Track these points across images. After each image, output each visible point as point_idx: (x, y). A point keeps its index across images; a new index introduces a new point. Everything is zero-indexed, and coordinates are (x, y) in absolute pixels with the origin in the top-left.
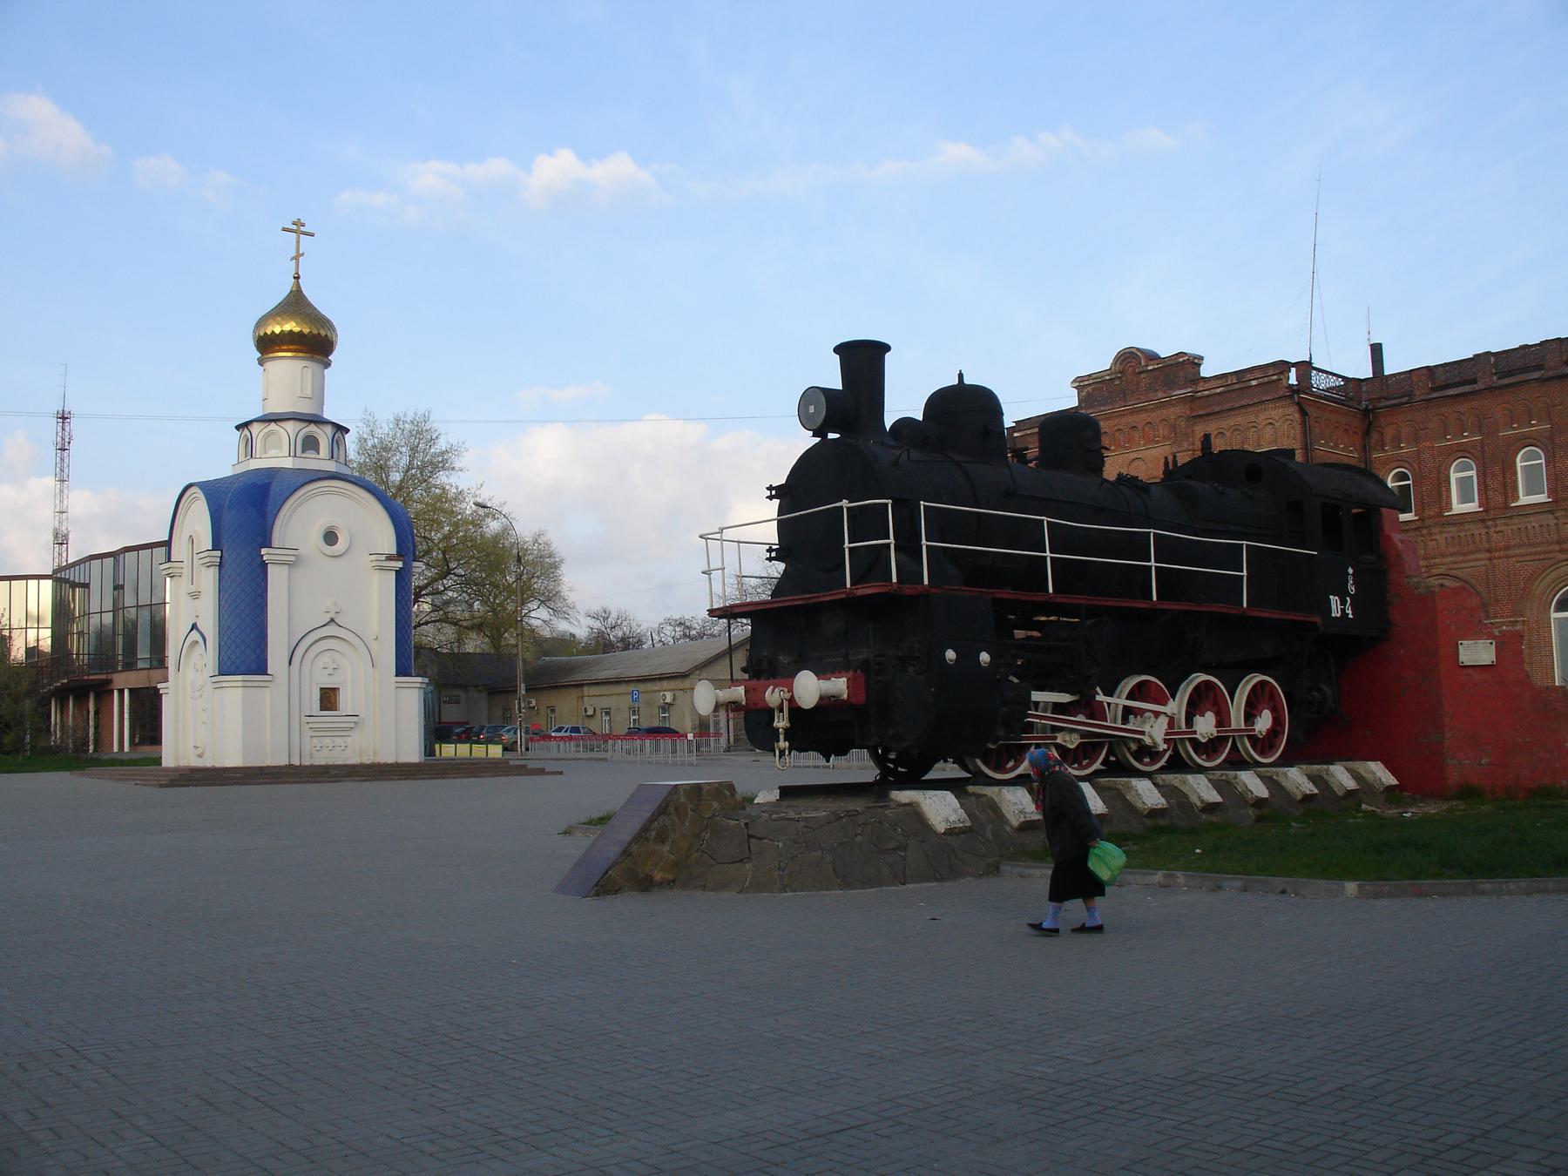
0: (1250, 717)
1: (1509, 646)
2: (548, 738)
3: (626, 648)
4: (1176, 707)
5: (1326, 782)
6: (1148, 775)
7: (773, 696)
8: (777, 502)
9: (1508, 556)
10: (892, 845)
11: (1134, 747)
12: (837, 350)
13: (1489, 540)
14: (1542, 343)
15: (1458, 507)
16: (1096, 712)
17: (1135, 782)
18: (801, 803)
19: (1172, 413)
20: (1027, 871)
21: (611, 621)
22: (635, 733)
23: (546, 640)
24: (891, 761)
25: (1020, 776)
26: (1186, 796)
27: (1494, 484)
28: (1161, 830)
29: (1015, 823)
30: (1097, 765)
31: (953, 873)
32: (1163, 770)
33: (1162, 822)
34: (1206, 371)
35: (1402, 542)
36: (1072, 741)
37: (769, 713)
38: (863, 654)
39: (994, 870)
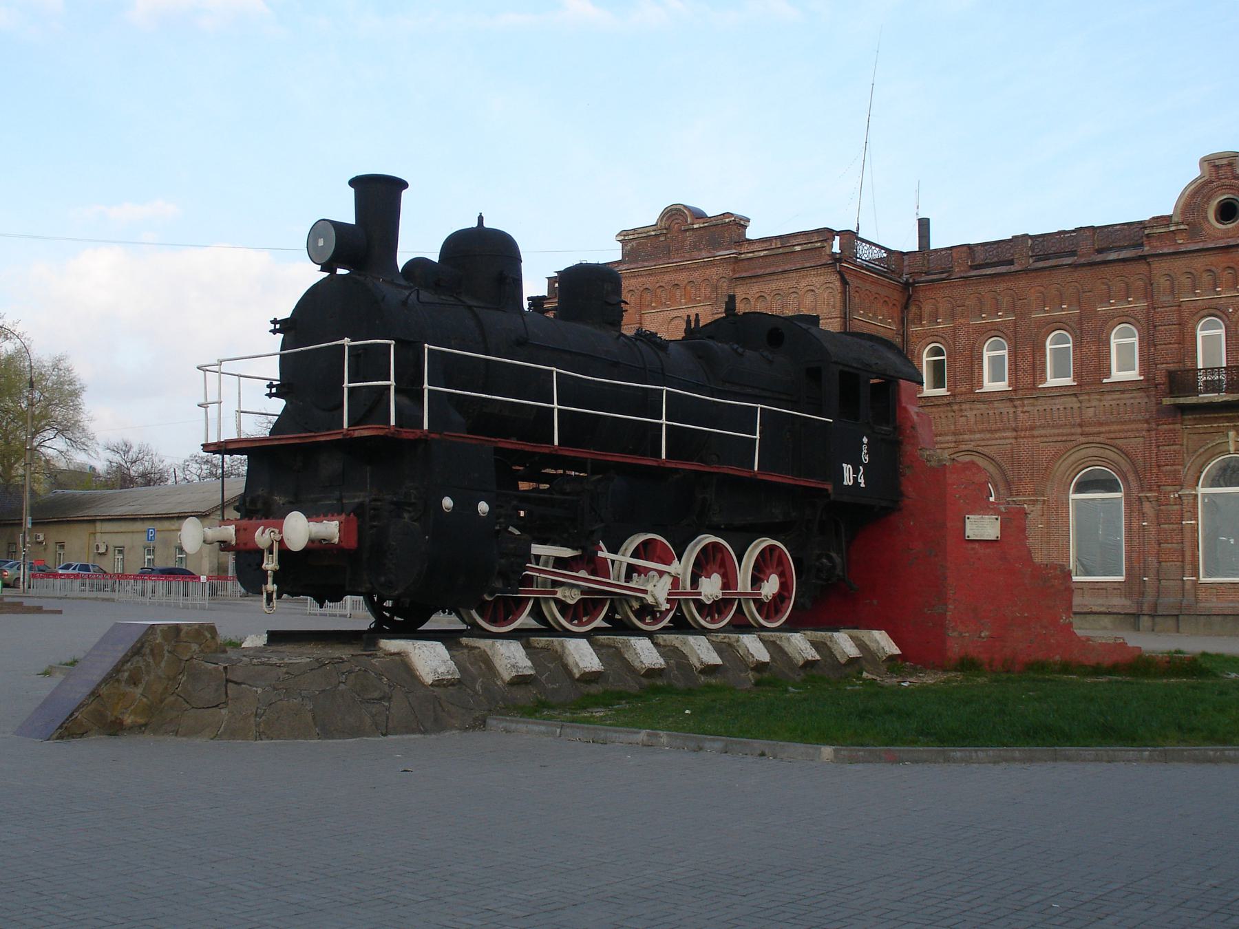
0: (757, 581)
1: (1013, 522)
2: (55, 575)
3: (148, 484)
4: (682, 567)
5: (829, 649)
6: (650, 635)
7: (263, 537)
8: (280, 336)
9: (1033, 437)
10: (376, 695)
11: (636, 605)
12: (354, 182)
13: (1016, 419)
14: (1077, 230)
15: (989, 385)
16: (599, 568)
17: (634, 640)
18: (286, 649)
19: (715, 273)
20: (513, 726)
21: (132, 455)
22: (147, 573)
23: (62, 472)
24: (387, 609)
25: (515, 630)
26: (685, 657)
27: (1024, 365)
28: (657, 690)
29: (507, 678)
30: (599, 622)
31: (439, 726)
32: (665, 630)
33: (659, 683)
34: (752, 233)
35: (918, 414)
36: (572, 597)
37: (259, 554)
38: (359, 498)
39: (481, 724)
